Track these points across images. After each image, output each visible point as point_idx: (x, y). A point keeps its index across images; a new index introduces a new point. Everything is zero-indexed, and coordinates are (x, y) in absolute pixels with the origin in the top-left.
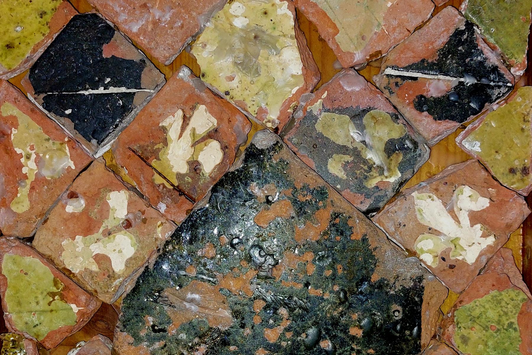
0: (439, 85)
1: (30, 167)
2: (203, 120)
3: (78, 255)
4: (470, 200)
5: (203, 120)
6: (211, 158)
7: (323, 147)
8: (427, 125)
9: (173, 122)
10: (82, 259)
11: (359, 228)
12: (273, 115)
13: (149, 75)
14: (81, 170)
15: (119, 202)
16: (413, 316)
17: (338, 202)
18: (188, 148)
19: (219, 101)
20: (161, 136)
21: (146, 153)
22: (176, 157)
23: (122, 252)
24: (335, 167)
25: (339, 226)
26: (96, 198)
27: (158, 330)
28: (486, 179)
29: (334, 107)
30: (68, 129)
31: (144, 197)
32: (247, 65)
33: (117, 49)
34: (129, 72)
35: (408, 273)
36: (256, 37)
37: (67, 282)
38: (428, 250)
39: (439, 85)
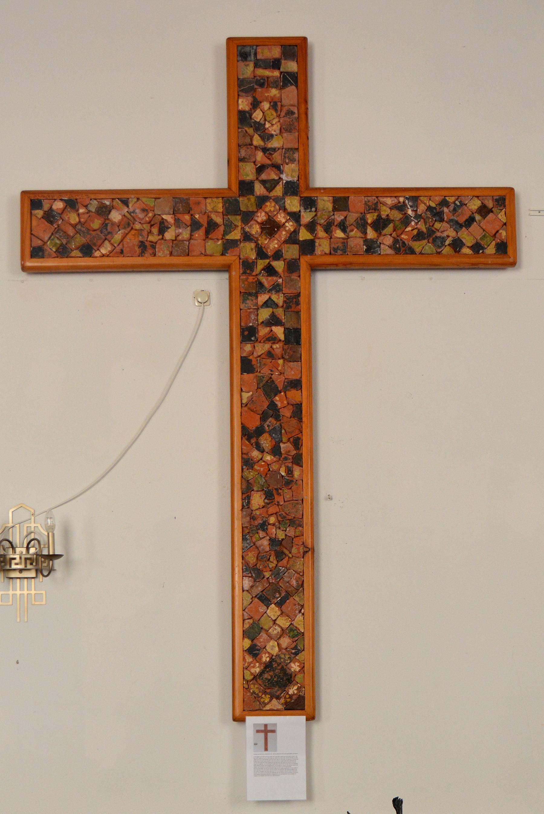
0: (293, 651)
1: (247, 661)
2: (267, 655)
3: (253, 670)
4: (297, 664)
5: (267, 655)
6: (268, 659)
7: (281, 658)
8: (293, 656)
9: (263, 655)
10: (49, 520)
11: (285, 667)
12: (275, 655)
13: (261, 650)
14: (72, 259)
15: (257, 664)
16: (291, 677)
17: (283, 664)
18: (265, 658)
19: (268, 653)
20: (262, 657)
21: (261, 659)
22: (264, 659)
23: (258, 670)
24: (282, 660)
25: (282, 667)
26: (255, 664)
27: (262, 679)
28: (299, 662)
29: (282, 653)
30: (251, 656)
31: (260, 664)
32: (272, 649)
33: (258, 647)
34: (259, 650)
35: (290, 672)
36: (273, 646)
37: (252, 674)
38: (293, 670)
39: (293, 651)
